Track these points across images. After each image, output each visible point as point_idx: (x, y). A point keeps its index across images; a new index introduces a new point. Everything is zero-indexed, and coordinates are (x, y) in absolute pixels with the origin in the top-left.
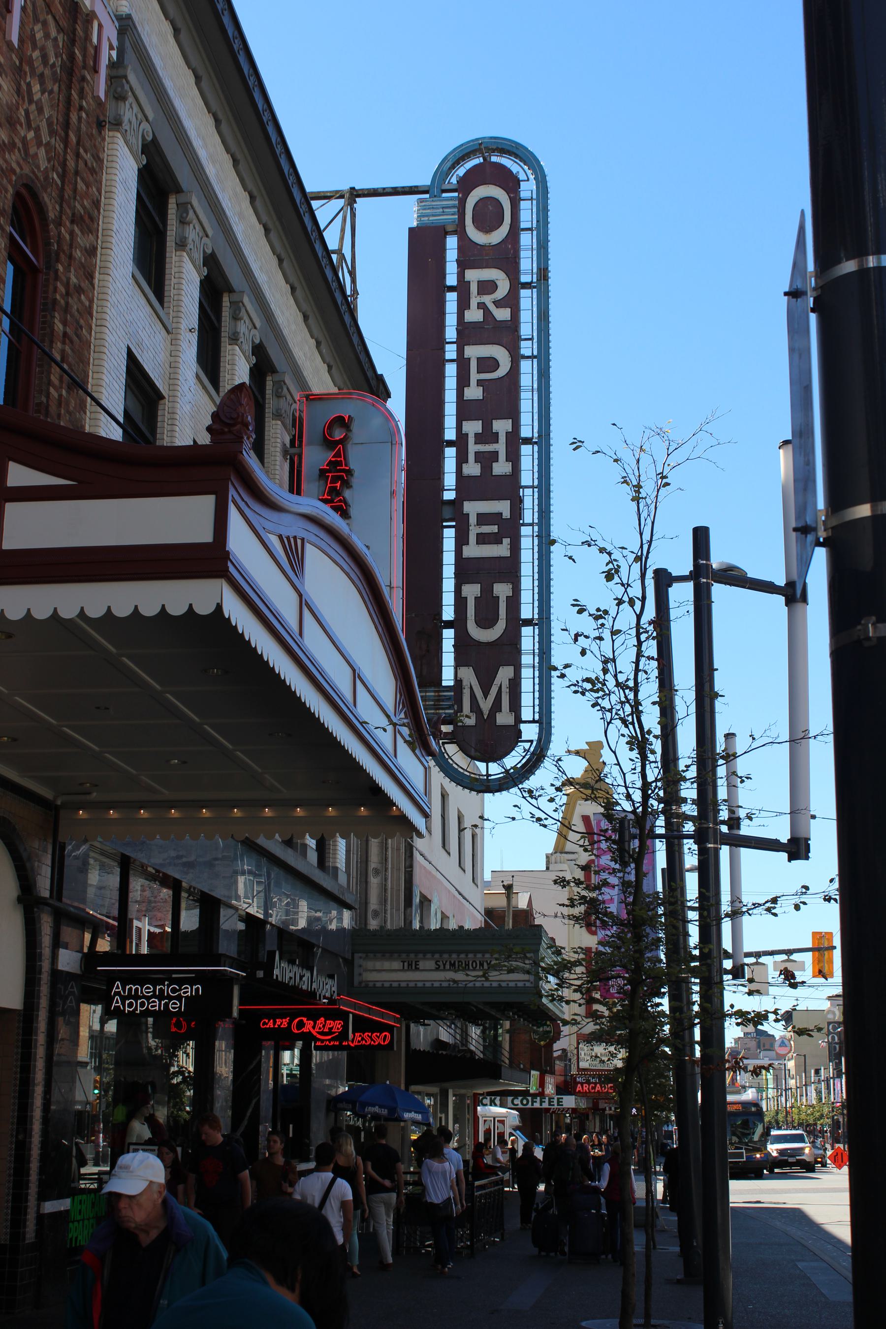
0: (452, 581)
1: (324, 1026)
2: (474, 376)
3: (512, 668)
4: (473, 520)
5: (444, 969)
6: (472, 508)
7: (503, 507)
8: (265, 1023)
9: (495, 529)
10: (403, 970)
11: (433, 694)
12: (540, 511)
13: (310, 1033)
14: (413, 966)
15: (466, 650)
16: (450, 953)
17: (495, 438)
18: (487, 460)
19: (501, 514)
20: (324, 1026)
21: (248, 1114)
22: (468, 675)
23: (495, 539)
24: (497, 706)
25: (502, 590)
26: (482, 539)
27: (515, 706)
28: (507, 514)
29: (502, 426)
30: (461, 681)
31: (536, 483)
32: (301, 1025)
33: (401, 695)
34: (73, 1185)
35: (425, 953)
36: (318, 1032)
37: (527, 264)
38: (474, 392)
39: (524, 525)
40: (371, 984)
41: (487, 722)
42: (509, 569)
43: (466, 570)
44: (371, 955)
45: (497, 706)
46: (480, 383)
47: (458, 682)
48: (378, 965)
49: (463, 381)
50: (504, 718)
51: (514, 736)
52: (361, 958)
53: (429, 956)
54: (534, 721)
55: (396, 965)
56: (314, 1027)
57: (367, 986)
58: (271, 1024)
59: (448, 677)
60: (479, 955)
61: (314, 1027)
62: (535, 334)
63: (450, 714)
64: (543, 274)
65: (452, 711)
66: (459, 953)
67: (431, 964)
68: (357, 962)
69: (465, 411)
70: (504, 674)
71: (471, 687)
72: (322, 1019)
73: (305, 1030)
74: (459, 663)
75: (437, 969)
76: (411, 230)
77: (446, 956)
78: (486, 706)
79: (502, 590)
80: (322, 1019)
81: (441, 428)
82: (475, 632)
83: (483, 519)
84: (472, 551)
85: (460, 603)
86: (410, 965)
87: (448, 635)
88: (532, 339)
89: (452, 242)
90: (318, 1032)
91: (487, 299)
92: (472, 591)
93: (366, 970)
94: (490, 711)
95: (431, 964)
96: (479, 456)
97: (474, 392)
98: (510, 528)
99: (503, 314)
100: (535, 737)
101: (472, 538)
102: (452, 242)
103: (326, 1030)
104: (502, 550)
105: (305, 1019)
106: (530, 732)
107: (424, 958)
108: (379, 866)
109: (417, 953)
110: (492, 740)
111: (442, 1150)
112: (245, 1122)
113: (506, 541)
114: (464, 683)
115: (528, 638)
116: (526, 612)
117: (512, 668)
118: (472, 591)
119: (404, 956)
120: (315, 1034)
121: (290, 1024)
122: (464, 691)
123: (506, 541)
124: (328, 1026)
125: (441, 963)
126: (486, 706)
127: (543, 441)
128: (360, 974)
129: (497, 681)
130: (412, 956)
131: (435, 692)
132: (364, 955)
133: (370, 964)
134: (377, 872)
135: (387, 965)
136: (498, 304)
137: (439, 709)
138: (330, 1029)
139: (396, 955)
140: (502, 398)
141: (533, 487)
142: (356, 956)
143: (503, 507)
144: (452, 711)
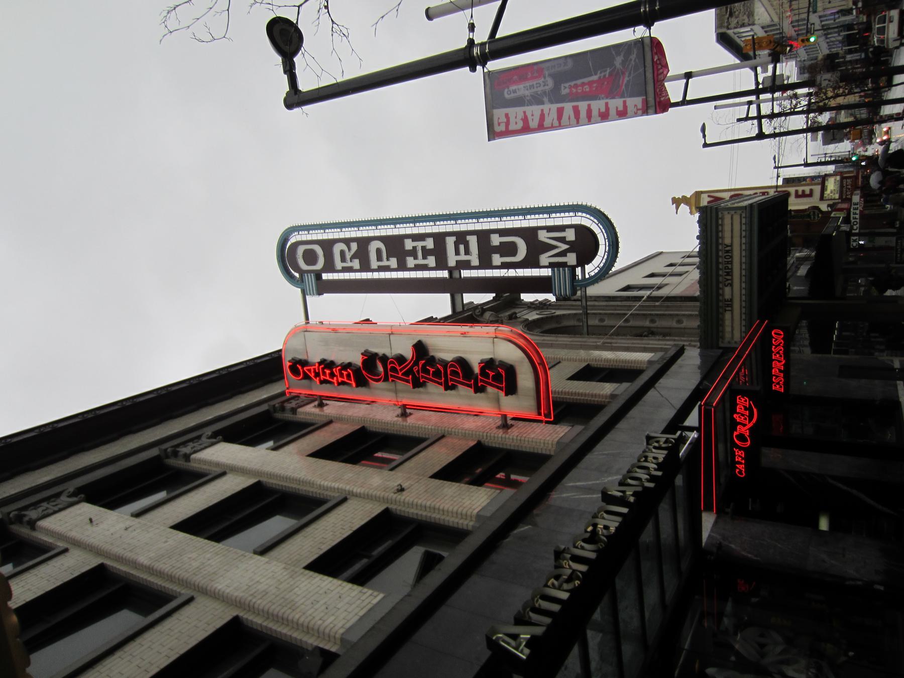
1: (743, 415)
2: (385, 263)
3: (492, 235)
5: (732, 280)
6: (452, 261)
7: (450, 241)
8: (740, 472)
10: (732, 311)
12: (351, 227)
13: (749, 429)
14: (729, 303)
15: (531, 261)
16: (718, 275)
17: (424, 258)
18: (426, 253)
20: (743, 415)
21: (845, 488)
22: (545, 259)
24: (562, 240)
25: (496, 240)
26: (467, 252)
27: (562, 228)
28: (453, 239)
32: (741, 437)
35: (718, 295)
36: (750, 422)
38: (393, 262)
41: (573, 247)
42: (484, 236)
43: (485, 263)
44: (721, 334)
45: (562, 240)
46: (388, 260)
47: (551, 265)
48: (728, 329)
49: (387, 269)
50: (570, 235)
51: (581, 230)
53: (721, 292)
55: (728, 315)
56: (744, 425)
58: (742, 467)
60: (720, 254)
61: (744, 425)
66: (718, 269)
67: (727, 290)
68: (725, 345)
69: (402, 267)
70: (543, 236)
72: (735, 416)
73: (747, 434)
74: (538, 266)
75: (731, 285)
77: (721, 279)
80: (735, 416)
83: (457, 253)
84: (475, 262)
85: (505, 266)
86: (728, 306)
89: (325, 276)
90: (750, 422)
91: (348, 257)
92: (497, 259)
95: (727, 290)
96: (424, 258)
97: (393, 262)
98: (461, 237)
99: (354, 246)
102: (325, 276)
103: (747, 413)
104: (473, 240)
105: (735, 433)
107: (723, 295)
108: (675, 319)
109: (718, 301)
110: (585, 245)
112: (855, 492)
117: (492, 235)
118: (497, 259)
120: (751, 425)
121: (740, 448)
123: (468, 238)
124: (743, 411)
125: (727, 283)
130: (721, 304)
133: (728, 336)
134: (679, 322)
135: (728, 323)
136: (349, 249)
138: (746, 408)
139: (721, 316)
140: (394, 245)
142: (721, 345)
143: (450, 241)
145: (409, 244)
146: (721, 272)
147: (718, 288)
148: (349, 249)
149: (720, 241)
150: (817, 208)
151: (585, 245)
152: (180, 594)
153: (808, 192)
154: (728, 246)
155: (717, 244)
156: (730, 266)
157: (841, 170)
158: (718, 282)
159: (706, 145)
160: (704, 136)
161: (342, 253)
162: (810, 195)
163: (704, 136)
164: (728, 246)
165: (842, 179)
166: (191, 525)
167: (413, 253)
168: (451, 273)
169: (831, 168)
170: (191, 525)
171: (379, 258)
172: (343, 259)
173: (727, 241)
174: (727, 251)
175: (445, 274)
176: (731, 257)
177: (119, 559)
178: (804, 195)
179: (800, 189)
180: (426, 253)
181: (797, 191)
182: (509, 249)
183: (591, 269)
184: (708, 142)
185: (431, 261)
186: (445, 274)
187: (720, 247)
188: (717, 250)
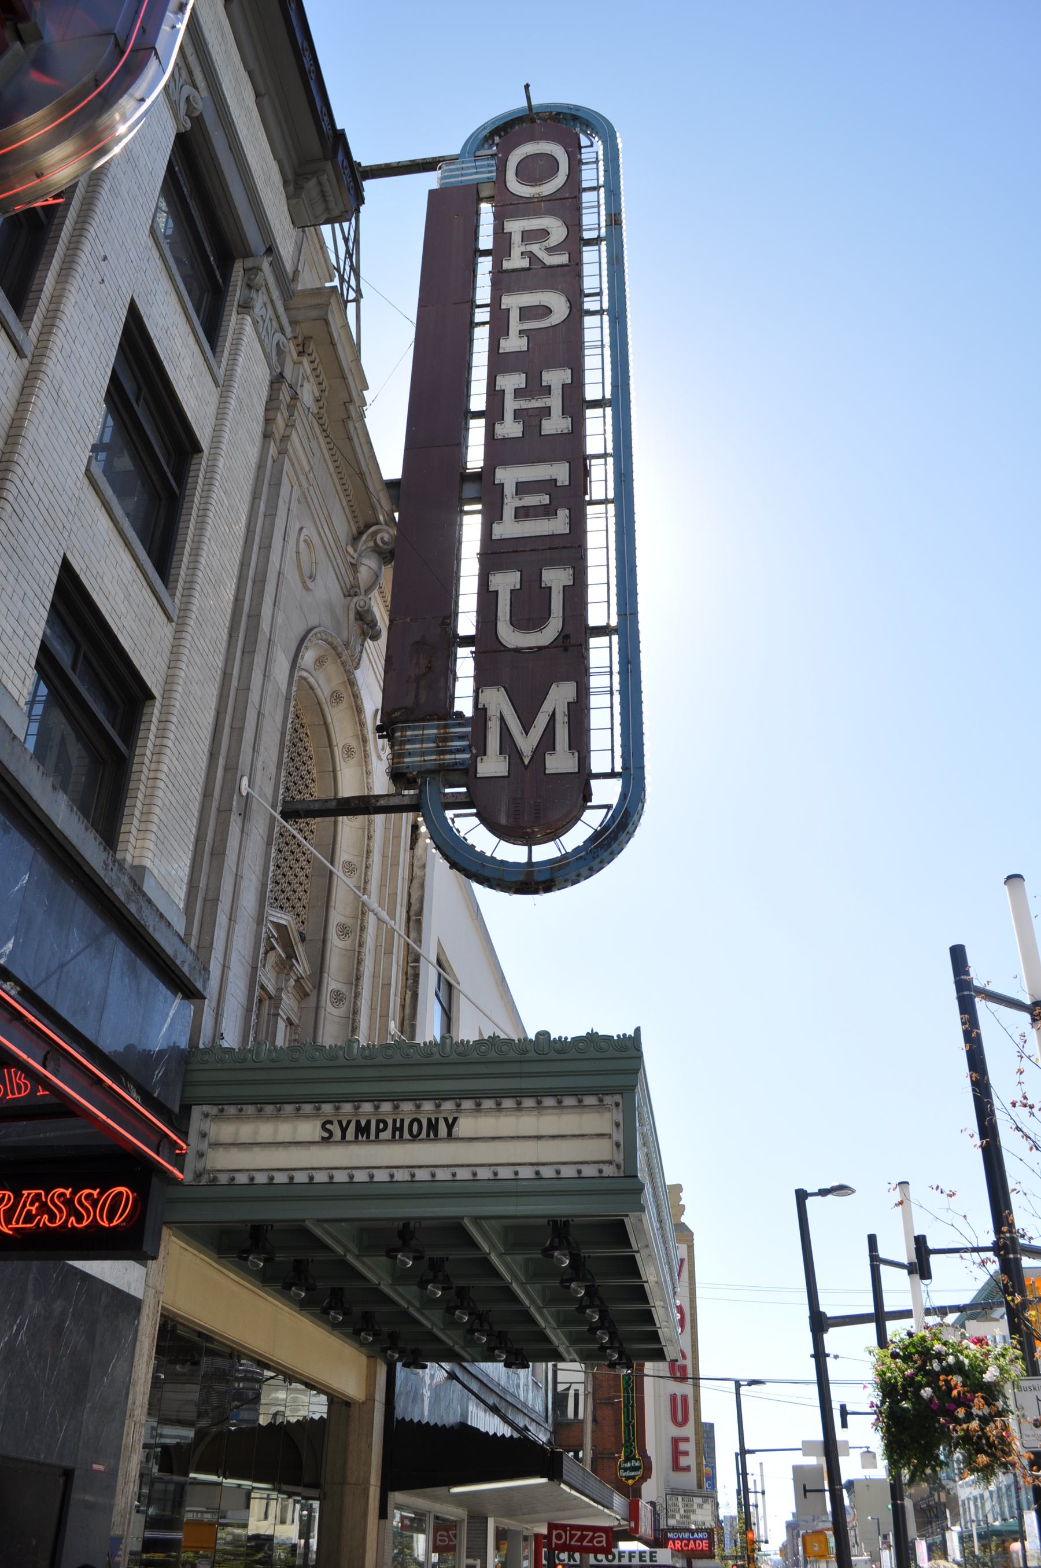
0: (471, 683)
4: (509, 490)
6: (508, 476)
7: (560, 472)
9: (545, 499)
11: (435, 731)
18: (532, 419)
19: (556, 480)
22: (497, 700)
23: (548, 512)
24: (548, 742)
25: (556, 578)
26: (523, 513)
29: (556, 378)
30: (485, 709)
31: (610, 450)
33: (346, 326)
34: (224, 1535)
37: (593, 219)
39: (592, 503)
40: (223, 1179)
41: (527, 770)
42: (572, 550)
43: (493, 556)
45: (548, 742)
47: (480, 711)
48: (246, 1131)
50: (560, 762)
51: (578, 788)
52: (206, 1115)
54: (612, 775)
55: (309, 1129)
57: (213, 1183)
59: (464, 704)
62: (605, 286)
63: (463, 762)
64: (614, 220)
65: (467, 756)
69: (498, 363)
70: (560, 695)
71: (502, 719)
74: (481, 680)
76: (432, 193)
77: (347, 1108)
78: (527, 744)
79: (556, 578)
81: (451, 616)
82: (510, 636)
83: (522, 488)
84: (508, 528)
85: (487, 598)
87: (485, 265)
88: (599, 294)
91: (535, 248)
92: (506, 582)
93: (216, 1145)
94: (535, 752)
97: (514, 343)
98: (573, 497)
100: (614, 801)
101: (508, 512)
104: (559, 524)
106: (606, 792)
110: (536, 801)
111: (468, 845)
113: (563, 514)
114: (490, 713)
115: (601, 654)
116: (598, 615)
118: (506, 582)
119: (327, 1108)
122: (490, 724)
123: (563, 514)
126: (527, 744)
127: (619, 402)
128: (201, 1155)
129: (547, 707)
131: (438, 727)
132: (213, 1110)
133: (225, 1131)
136: (550, 250)
137: (444, 753)
139: (308, 1108)
141: (605, 456)
143: (560, 472)
144: (467, 756)
145: (556, 378)
146: (367, 1107)
147: (318, 1101)
148: (550, 250)
149: (467, 1104)
150: (647, 1474)
151: (536, 801)
152: (27, 329)
153: (683, 1461)
154: (450, 1127)
155: (458, 1097)
156: (386, 1135)
157: (727, 1530)
158: (337, 1100)
159: (801, 1196)
160: (823, 1192)
161: (543, 234)
162: (676, 1467)
163: (823, 1192)
164: (450, 1127)
165: (710, 1532)
166: (136, 342)
167: (535, 388)
168: (477, 477)
169: (728, 1506)
170: (136, 342)
171: (526, 313)
172: (528, 236)
173: (465, 1126)
174: (433, 1126)
175: (475, 458)
176: (415, 1138)
177: (212, 469)
178: (677, 1454)
179: (690, 1447)
180: (532, 419)
181: (686, 1440)
182: (530, 608)
183: (471, 830)
184: (810, 1202)
185: (510, 428)
186: (475, 458)
187: (449, 1105)
188: (438, 1098)
